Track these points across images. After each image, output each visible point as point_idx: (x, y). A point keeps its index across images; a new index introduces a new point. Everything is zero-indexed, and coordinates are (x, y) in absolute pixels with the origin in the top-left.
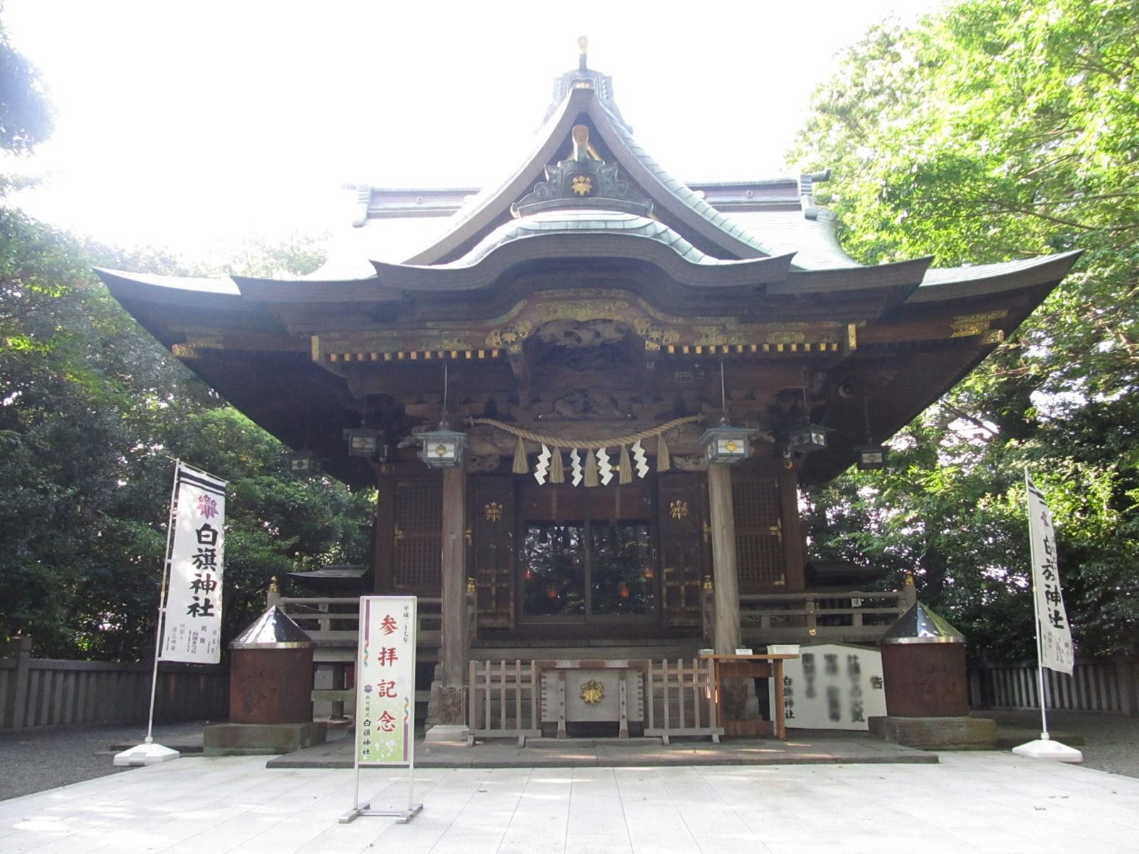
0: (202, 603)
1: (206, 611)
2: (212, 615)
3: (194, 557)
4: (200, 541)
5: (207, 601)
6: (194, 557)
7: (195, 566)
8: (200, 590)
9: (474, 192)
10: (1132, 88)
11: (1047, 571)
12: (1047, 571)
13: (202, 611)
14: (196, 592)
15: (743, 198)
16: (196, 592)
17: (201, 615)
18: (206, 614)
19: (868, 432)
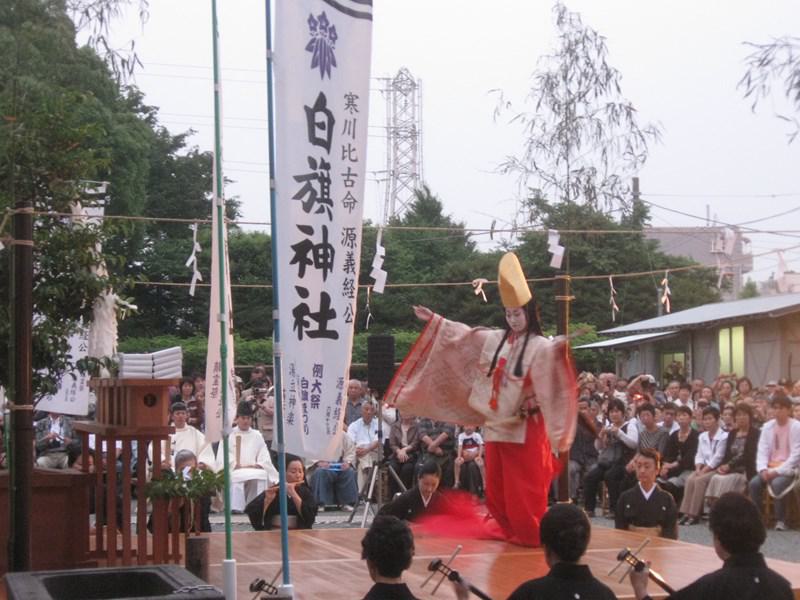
0: (314, 306)
1: (323, 325)
2: (334, 335)
3: (299, 179)
4: (346, 186)
5: (325, 299)
6: (299, 179)
7: (299, 204)
8: (309, 269)
9: (331, 219)
10: (23, 424)
11: (308, 187)
12: (308, 187)
13: (314, 326)
14: (301, 274)
15: (163, 359)
16: (301, 274)
17: (312, 334)
18: (323, 333)
19: (100, 272)
